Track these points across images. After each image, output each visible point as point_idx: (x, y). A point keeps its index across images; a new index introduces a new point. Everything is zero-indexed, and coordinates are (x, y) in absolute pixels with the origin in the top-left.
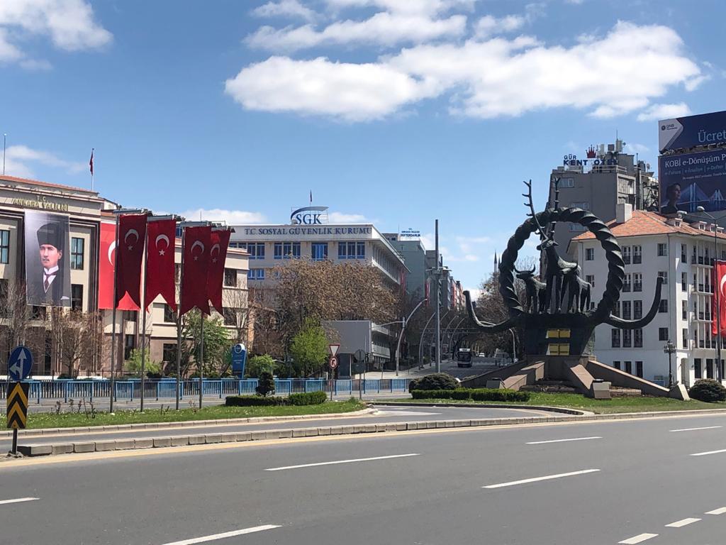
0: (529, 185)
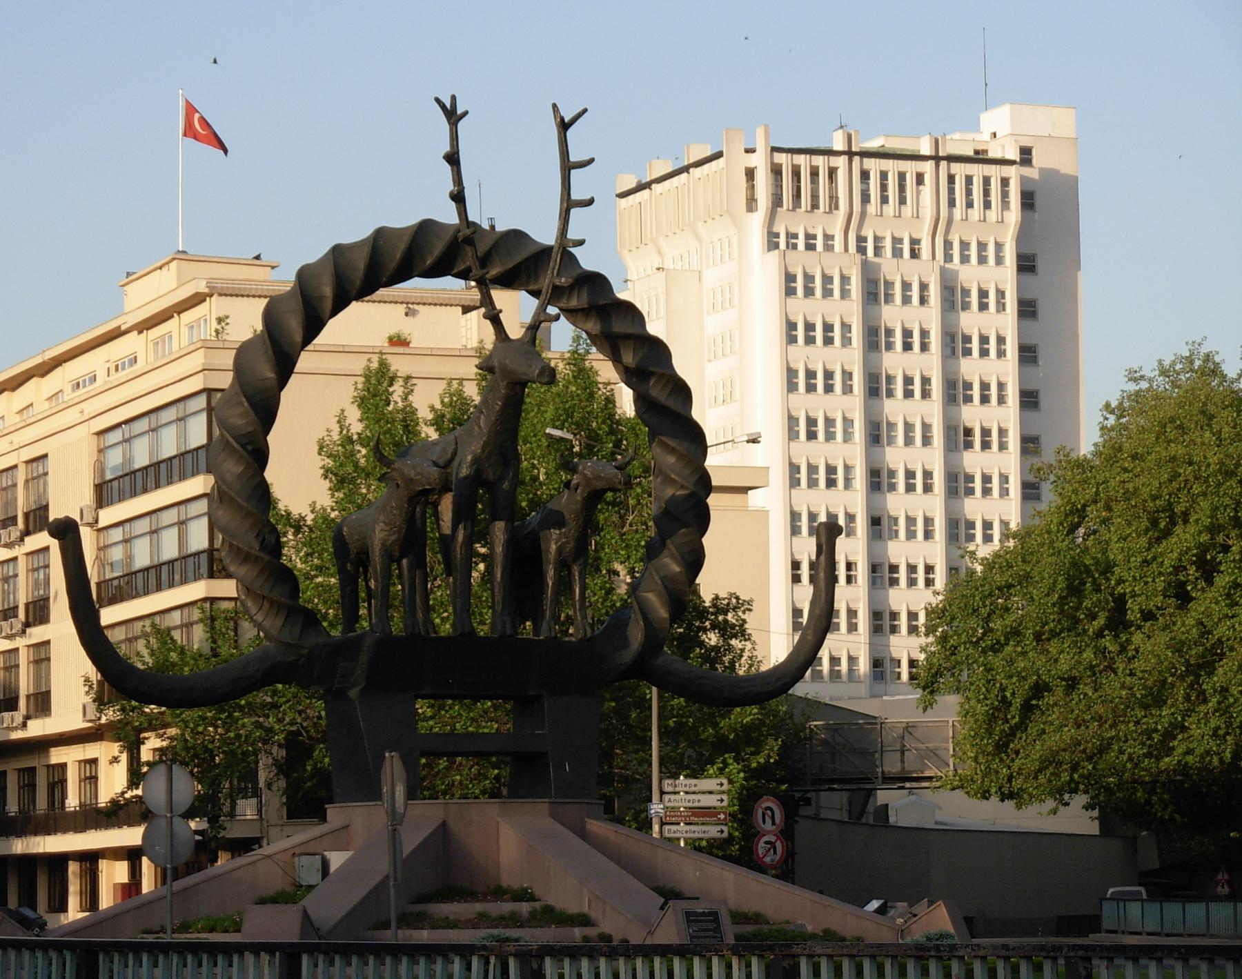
0: (453, 115)
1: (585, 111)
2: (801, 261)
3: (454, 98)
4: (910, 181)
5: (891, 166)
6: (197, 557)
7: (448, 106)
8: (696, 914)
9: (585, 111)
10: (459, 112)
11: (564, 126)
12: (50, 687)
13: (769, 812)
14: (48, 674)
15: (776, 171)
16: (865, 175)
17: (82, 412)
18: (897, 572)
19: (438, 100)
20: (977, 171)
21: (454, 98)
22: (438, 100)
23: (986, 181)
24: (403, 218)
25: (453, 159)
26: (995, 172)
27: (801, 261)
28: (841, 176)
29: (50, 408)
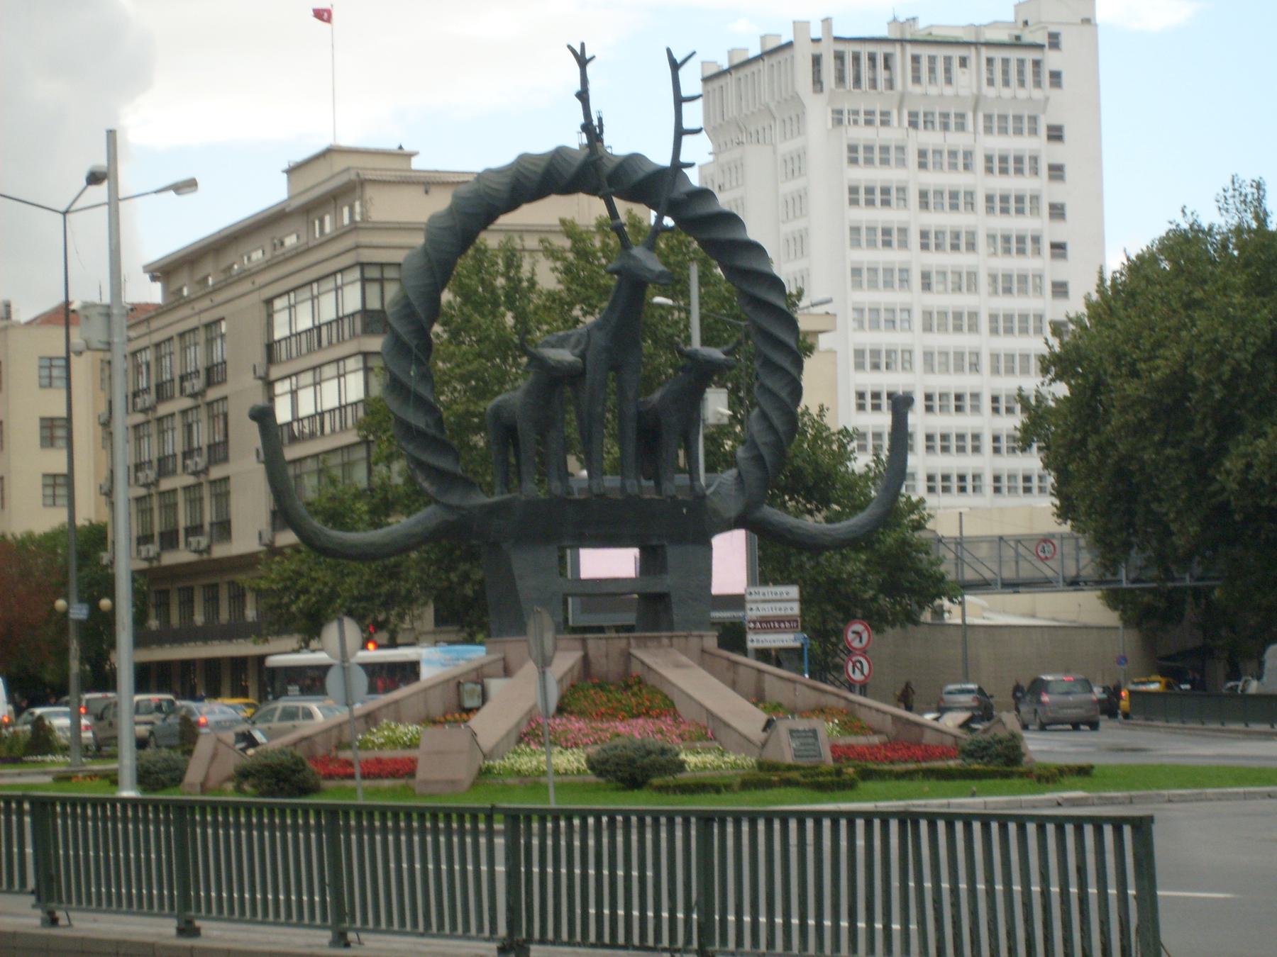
1: (694, 53)
2: (862, 134)
3: (583, 45)
4: (956, 63)
5: (940, 53)
6: (318, 370)
7: (578, 51)
8: (798, 731)
9: (694, 53)
10: (588, 56)
11: (675, 66)
12: (228, 513)
13: (858, 665)
14: (227, 505)
15: (839, 57)
16: (916, 59)
17: (253, 283)
18: (949, 440)
19: (569, 47)
20: (1014, 55)
21: (583, 45)
22: (569, 47)
23: (1021, 62)
24: (541, 145)
25: (583, 96)
26: (1029, 56)
27: (862, 134)
28: (897, 62)
29: (320, 366)
